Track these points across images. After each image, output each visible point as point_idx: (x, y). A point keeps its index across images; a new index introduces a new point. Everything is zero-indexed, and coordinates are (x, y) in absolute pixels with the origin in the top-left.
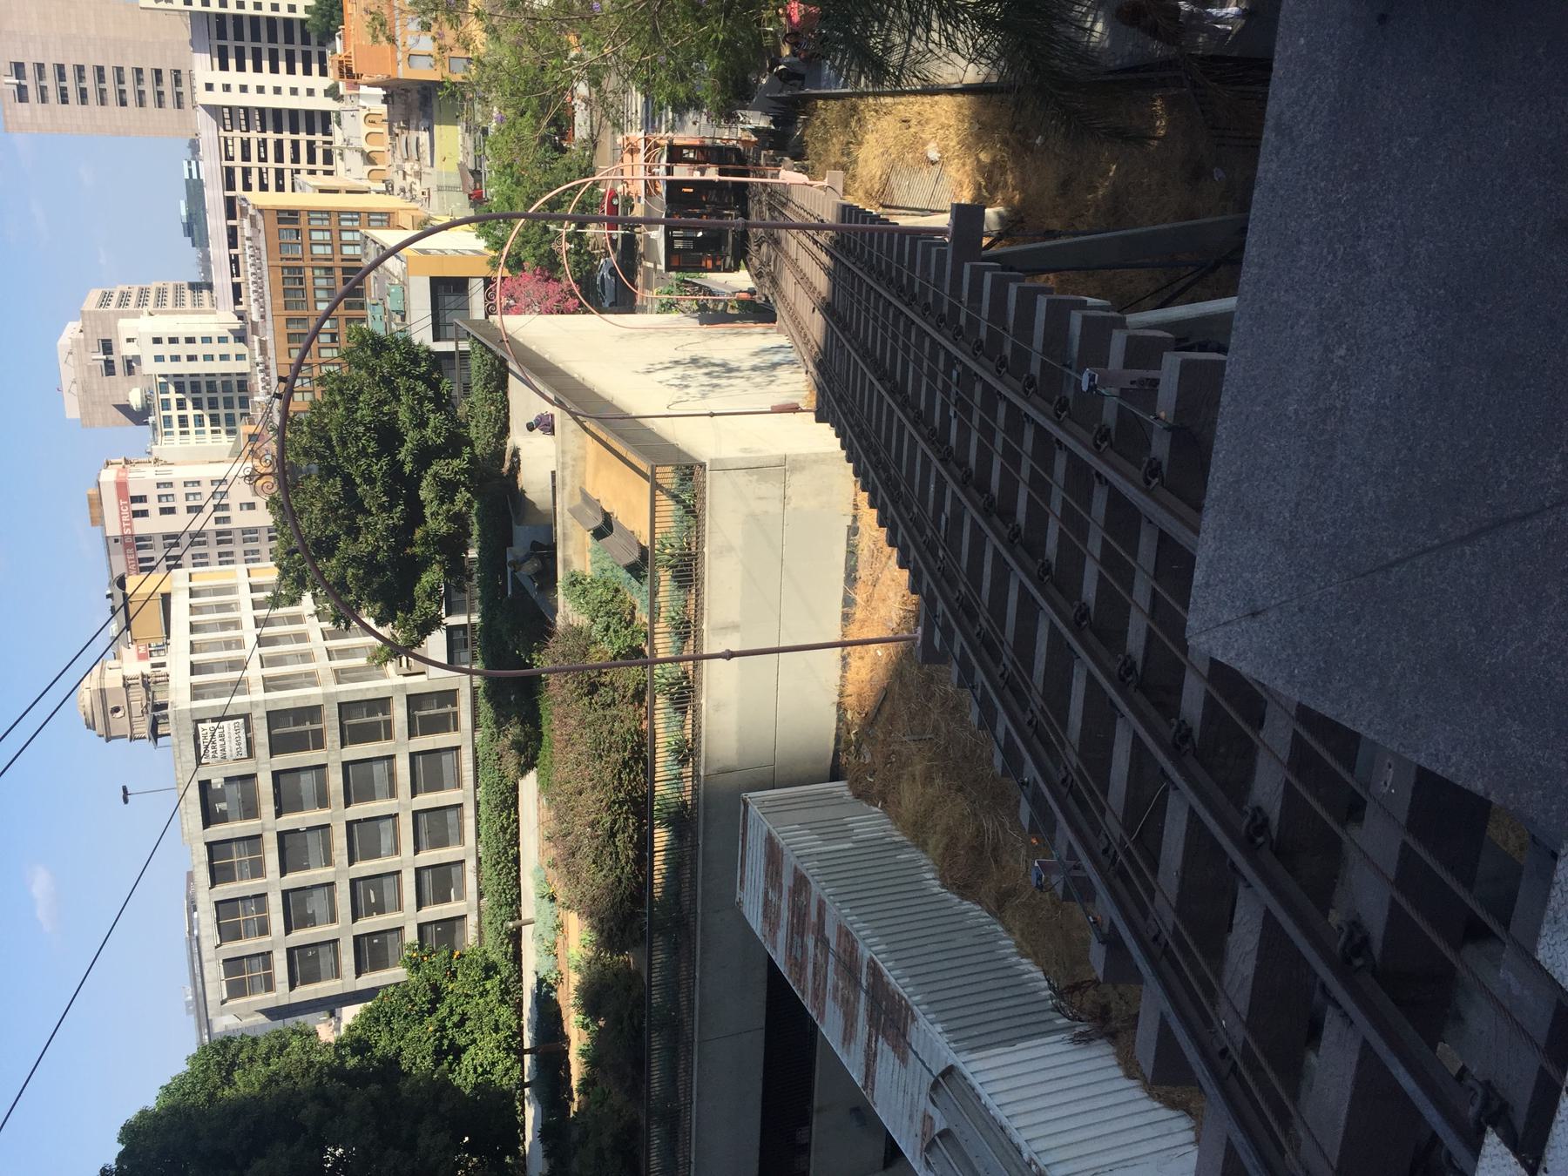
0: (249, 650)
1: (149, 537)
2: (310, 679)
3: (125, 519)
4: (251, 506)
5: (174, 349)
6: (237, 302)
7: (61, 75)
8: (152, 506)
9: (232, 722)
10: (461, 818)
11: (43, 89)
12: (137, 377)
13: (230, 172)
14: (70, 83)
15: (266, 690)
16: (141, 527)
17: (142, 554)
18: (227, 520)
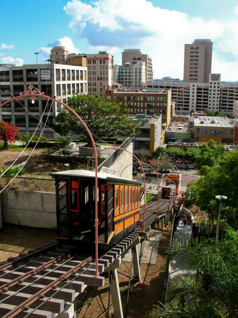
0: (66, 82)
2: (59, 94)
3: (100, 59)
5: (138, 72)
6: (148, 86)
7: (195, 68)
9: (50, 77)
11: (193, 72)
12: (132, 64)
13: (176, 88)
14: (194, 58)
15: (57, 85)
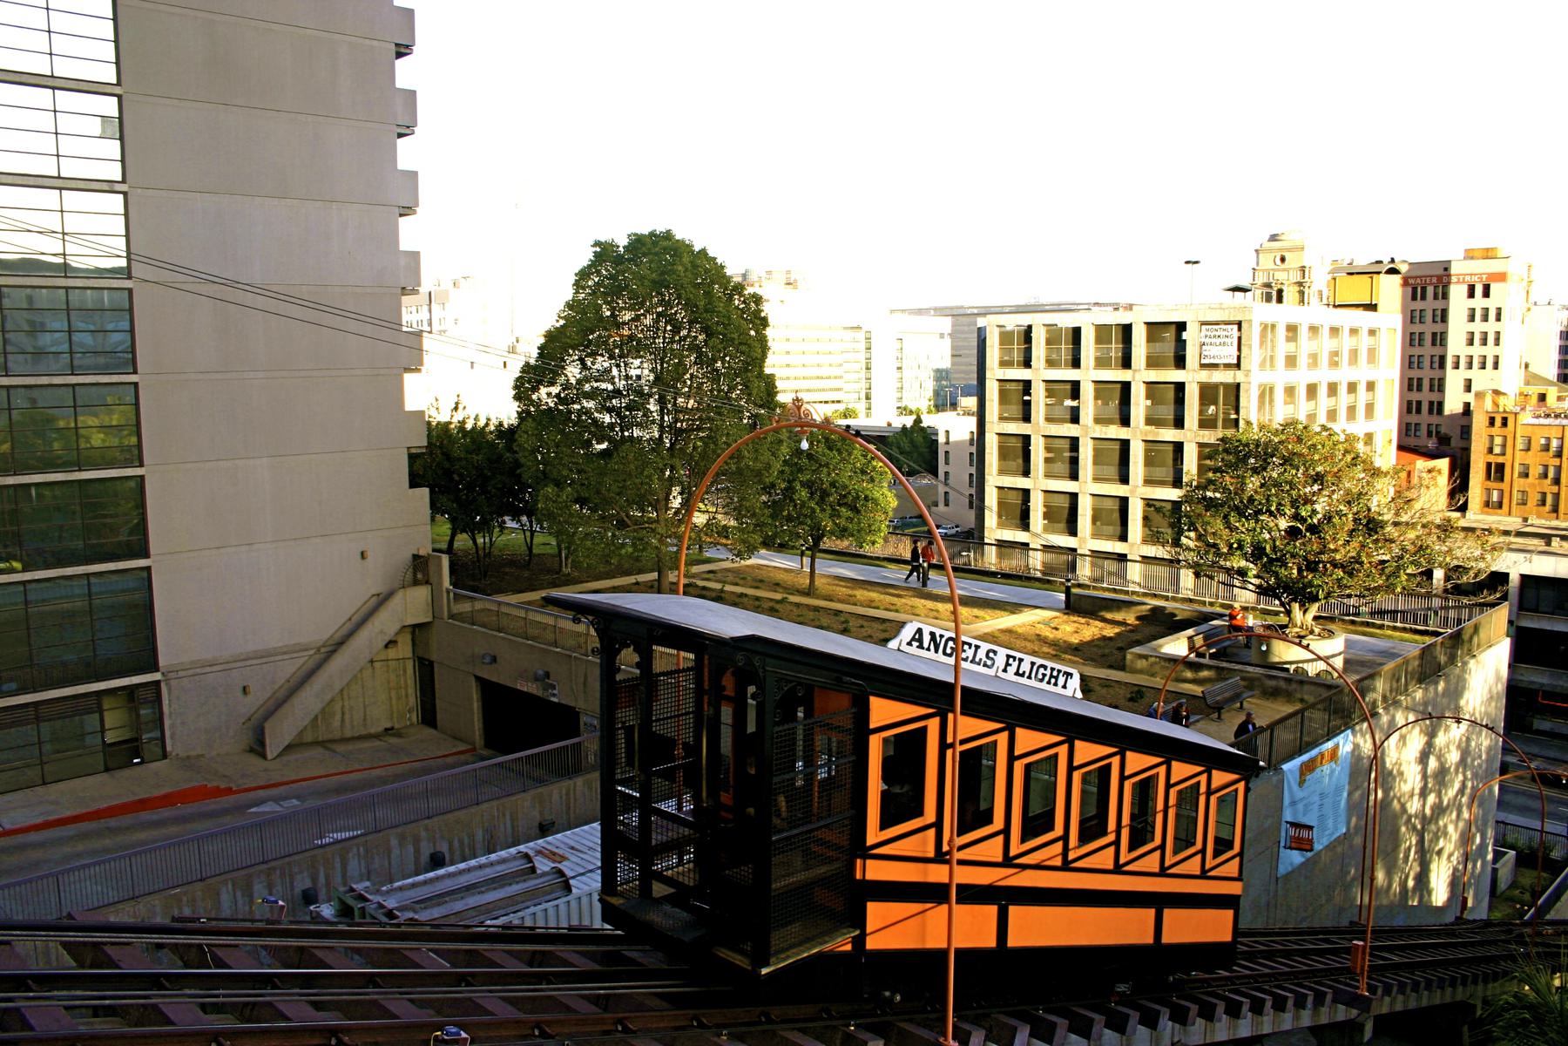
1: (1445, 296)
3: (1468, 278)
4: (1468, 388)
8: (1479, 302)
10: (1109, 537)
16: (1457, 293)
17: (1430, 290)
18: (1457, 366)
